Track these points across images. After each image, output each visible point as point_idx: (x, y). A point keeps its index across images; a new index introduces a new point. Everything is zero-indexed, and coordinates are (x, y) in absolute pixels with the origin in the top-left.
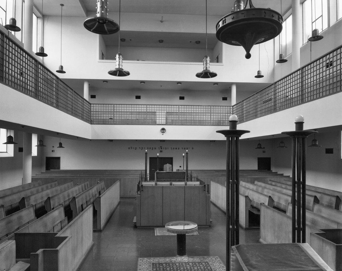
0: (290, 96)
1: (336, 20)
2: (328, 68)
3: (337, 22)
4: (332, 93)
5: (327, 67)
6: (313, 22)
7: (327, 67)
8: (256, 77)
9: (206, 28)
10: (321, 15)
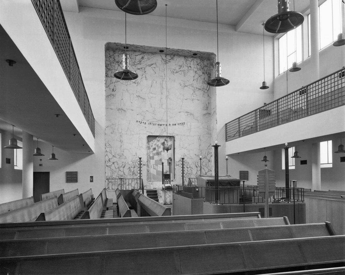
0: (297, 107)
1: (308, 56)
2: (301, 96)
3: (308, 58)
4: (321, 111)
5: (300, 94)
6: (288, 56)
7: (300, 94)
8: (261, 88)
9: (217, 28)
10: (288, 57)
